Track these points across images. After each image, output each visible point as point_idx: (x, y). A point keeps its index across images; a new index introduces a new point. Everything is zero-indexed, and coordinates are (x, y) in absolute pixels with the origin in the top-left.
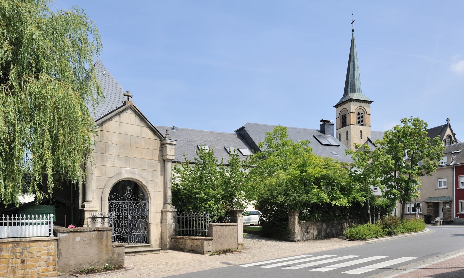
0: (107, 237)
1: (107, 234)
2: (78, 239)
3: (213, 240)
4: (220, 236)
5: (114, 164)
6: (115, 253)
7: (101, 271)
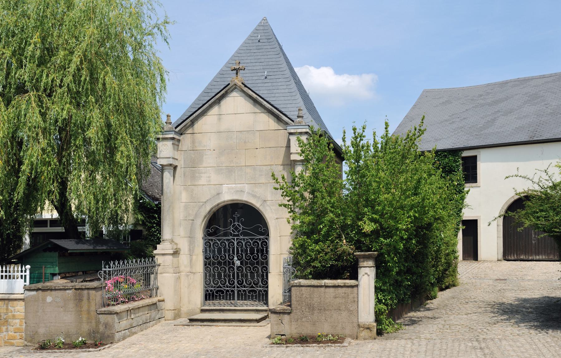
0: (89, 298)
1: (88, 294)
2: (49, 299)
3: (292, 315)
4: (311, 308)
5: (209, 181)
6: (100, 323)
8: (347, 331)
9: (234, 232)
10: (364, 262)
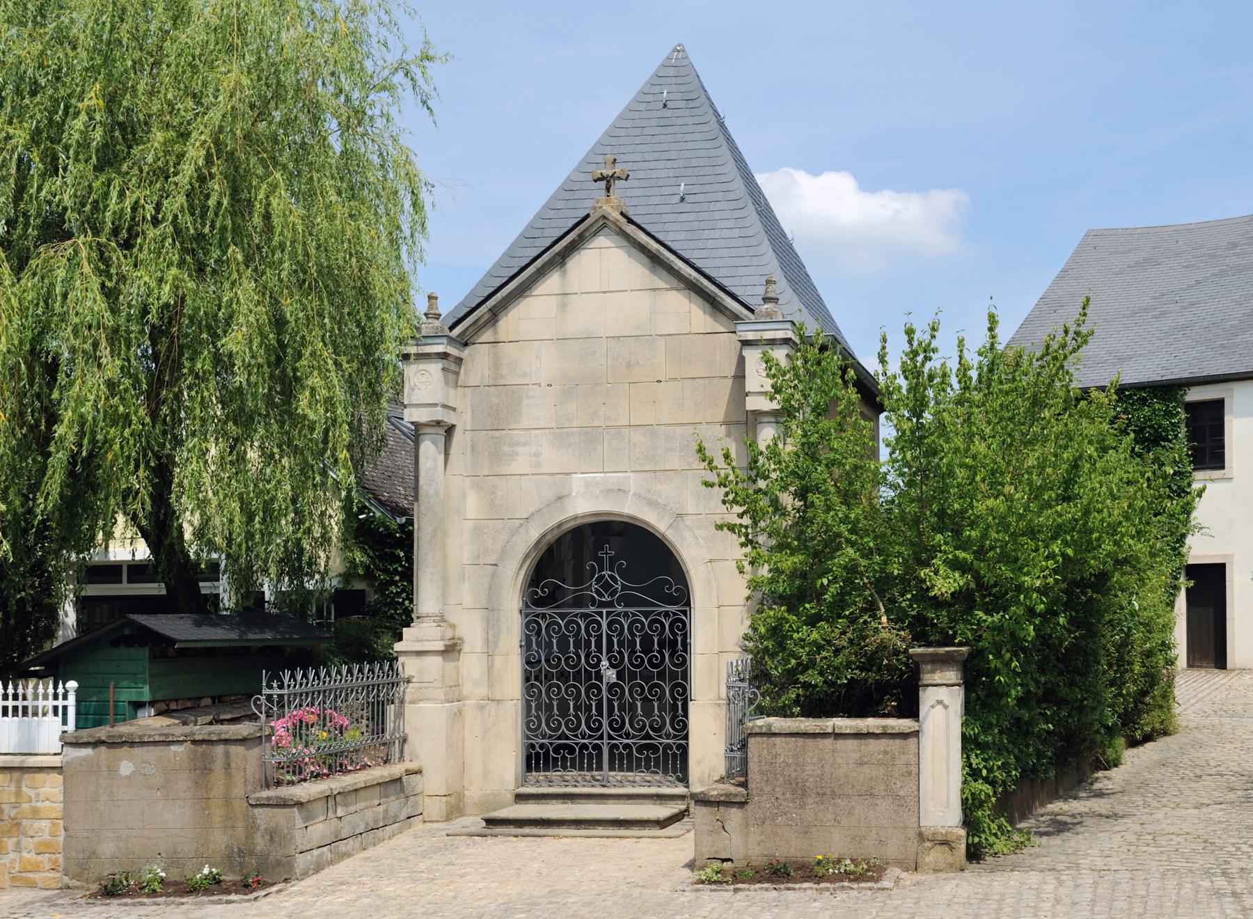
0: (229, 765)
1: (227, 755)
2: (126, 768)
3: (748, 808)
4: (799, 790)
5: (538, 464)
6: (258, 829)
7: (753, 880)
8: (892, 851)
9: (600, 595)
10: (933, 671)
